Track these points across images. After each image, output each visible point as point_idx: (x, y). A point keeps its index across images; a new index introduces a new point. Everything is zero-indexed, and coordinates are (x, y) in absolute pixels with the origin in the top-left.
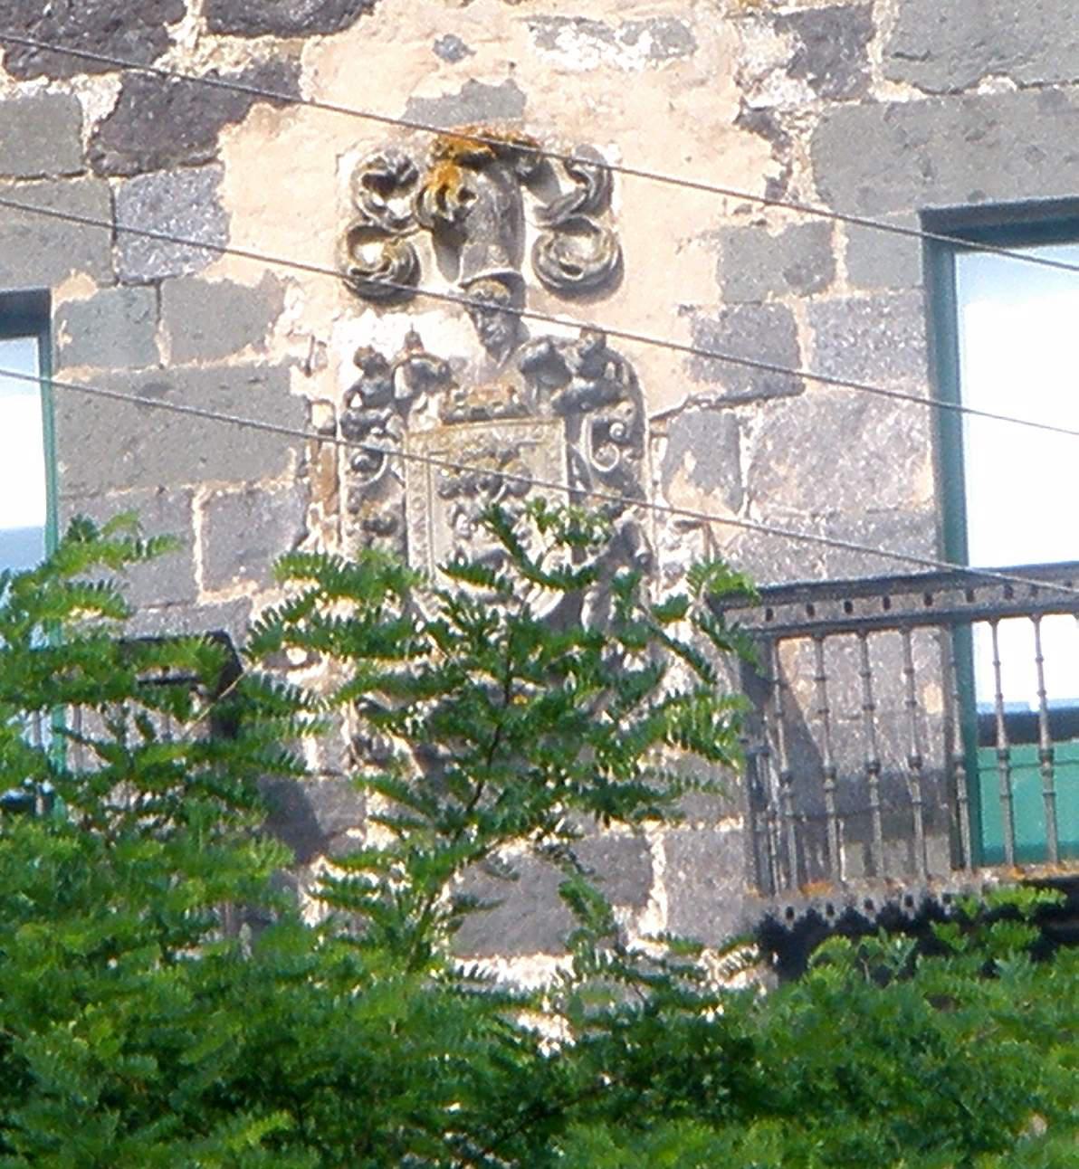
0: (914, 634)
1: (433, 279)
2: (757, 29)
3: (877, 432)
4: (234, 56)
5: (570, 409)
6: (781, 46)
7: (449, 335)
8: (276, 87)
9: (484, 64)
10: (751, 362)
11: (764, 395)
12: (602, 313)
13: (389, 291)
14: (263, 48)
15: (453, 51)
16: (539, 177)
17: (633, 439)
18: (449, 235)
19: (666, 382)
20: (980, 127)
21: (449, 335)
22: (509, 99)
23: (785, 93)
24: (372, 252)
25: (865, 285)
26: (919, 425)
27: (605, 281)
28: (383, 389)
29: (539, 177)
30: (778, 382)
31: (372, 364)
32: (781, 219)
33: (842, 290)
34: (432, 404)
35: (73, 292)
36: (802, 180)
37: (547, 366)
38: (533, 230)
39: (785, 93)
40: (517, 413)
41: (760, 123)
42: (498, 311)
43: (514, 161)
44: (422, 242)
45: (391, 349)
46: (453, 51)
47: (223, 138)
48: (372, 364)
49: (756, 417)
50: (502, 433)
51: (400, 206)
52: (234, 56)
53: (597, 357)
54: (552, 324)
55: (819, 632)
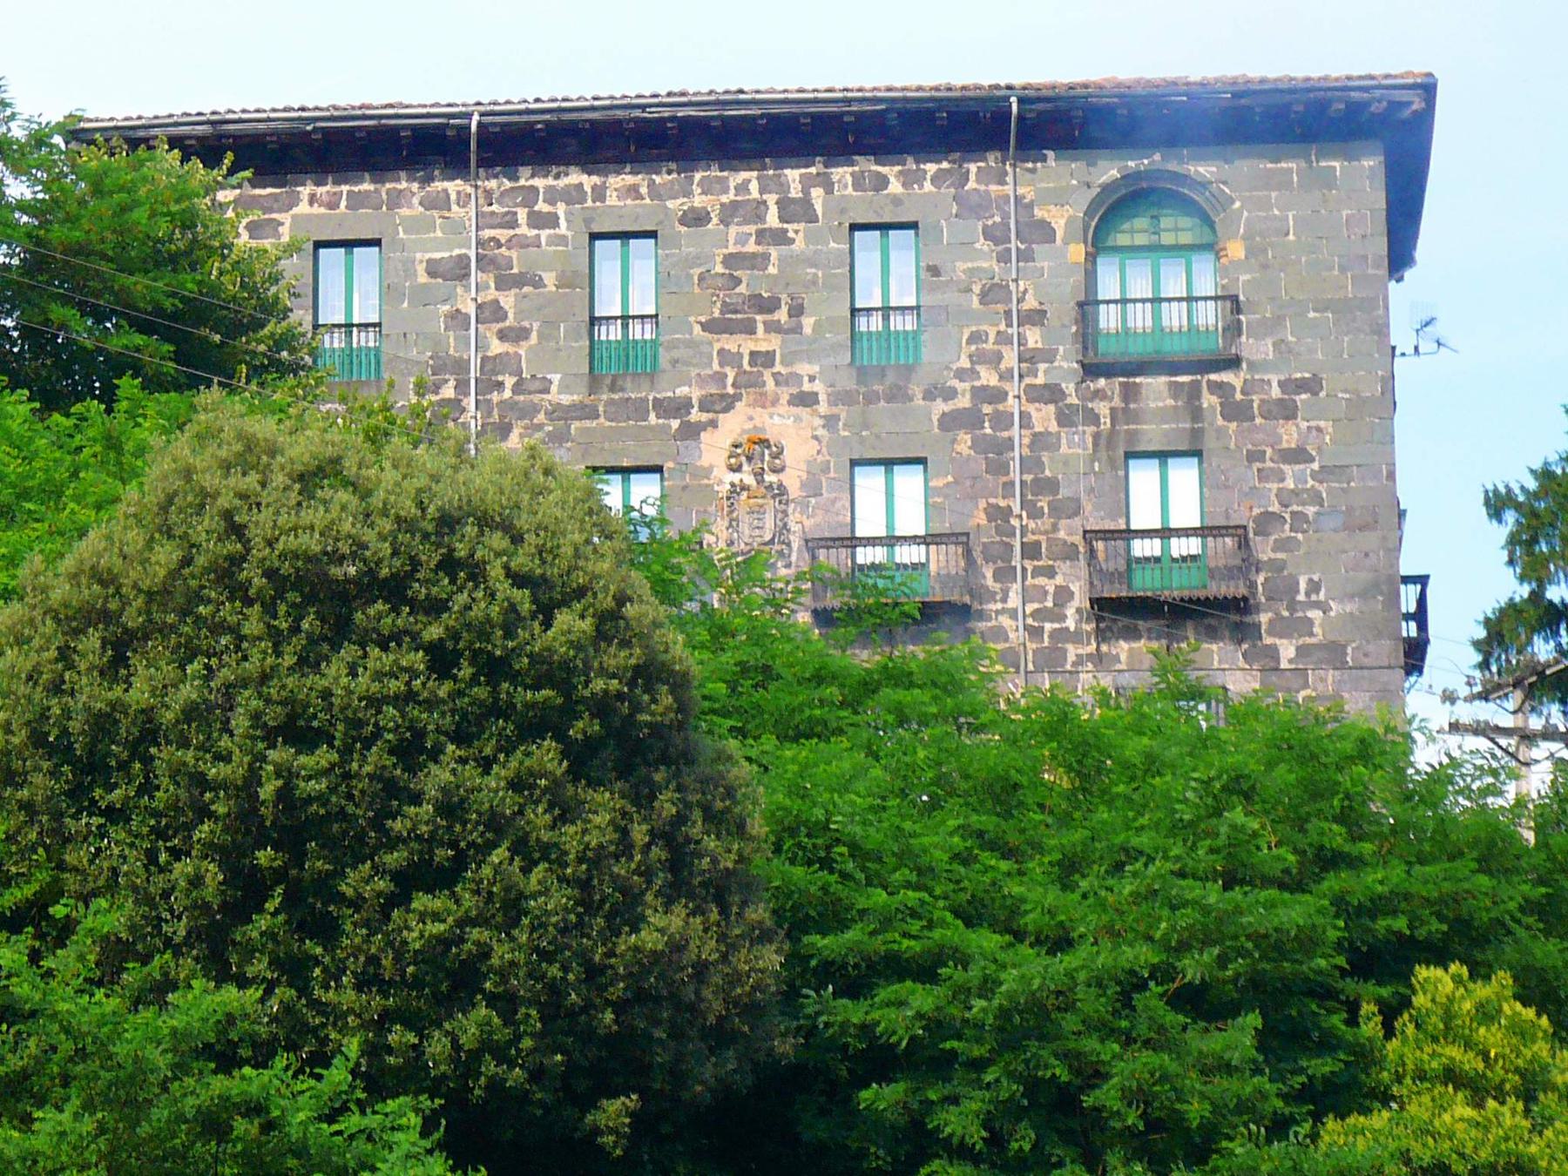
0: (897, 549)
1: (746, 467)
2: (822, 745)
3: (838, 505)
4: (705, 417)
5: (774, 497)
6: (820, 422)
7: (749, 480)
8: (713, 424)
9: (758, 422)
10: (812, 487)
11: (815, 495)
12: (782, 476)
13: (737, 469)
14: (711, 415)
15: (751, 418)
16: (769, 447)
17: (787, 503)
18: (749, 459)
19: (794, 490)
20: (862, 440)
21: (749, 480)
22: (763, 430)
23: (821, 432)
24: (733, 461)
25: (838, 471)
26: (848, 505)
27: (782, 469)
28: (736, 490)
29: (769, 447)
30: (818, 494)
31: (733, 485)
32: (820, 458)
33: (832, 475)
34: (745, 494)
35: (668, 465)
36: (824, 450)
37: (770, 487)
38: (767, 458)
39: (821, 432)
40: (763, 497)
41: (816, 438)
42: (759, 475)
43: (764, 443)
44: (743, 459)
45: (737, 482)
46: (751, 418)
47: (702, 434)
48: (733, 485)
49: (813, 500)
50: (760, 501)
51: (739, 451)
52: (705, 417)
53: (780, 486)
54: (770, 478)
55: (828, 548)
